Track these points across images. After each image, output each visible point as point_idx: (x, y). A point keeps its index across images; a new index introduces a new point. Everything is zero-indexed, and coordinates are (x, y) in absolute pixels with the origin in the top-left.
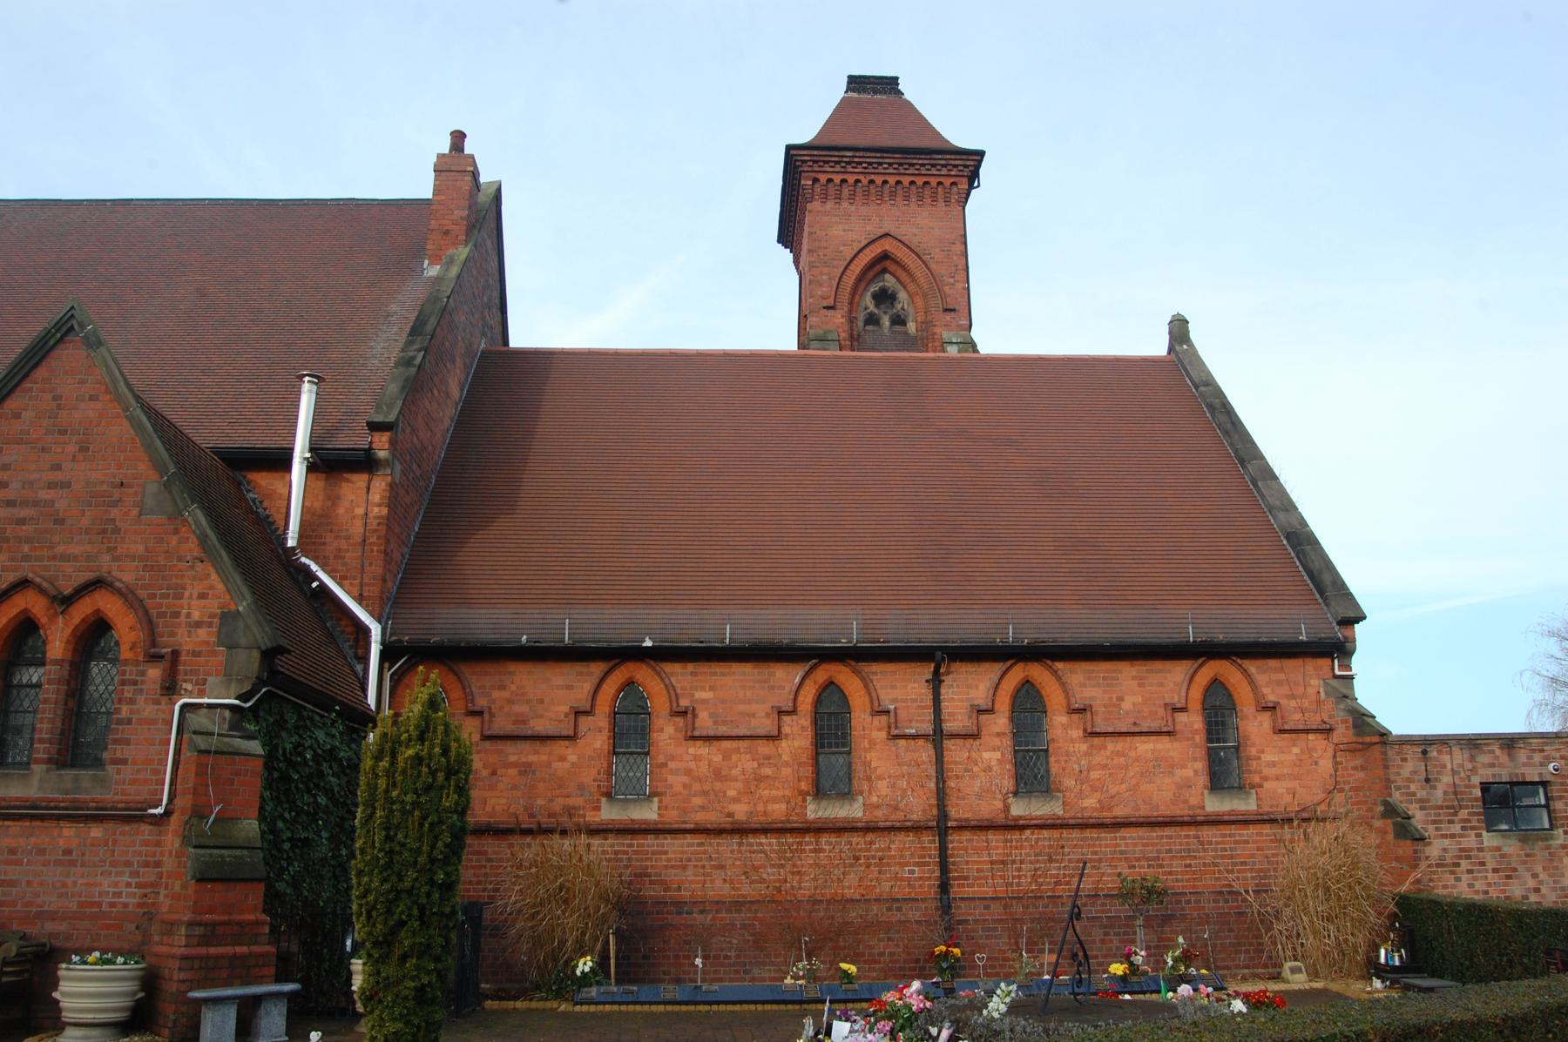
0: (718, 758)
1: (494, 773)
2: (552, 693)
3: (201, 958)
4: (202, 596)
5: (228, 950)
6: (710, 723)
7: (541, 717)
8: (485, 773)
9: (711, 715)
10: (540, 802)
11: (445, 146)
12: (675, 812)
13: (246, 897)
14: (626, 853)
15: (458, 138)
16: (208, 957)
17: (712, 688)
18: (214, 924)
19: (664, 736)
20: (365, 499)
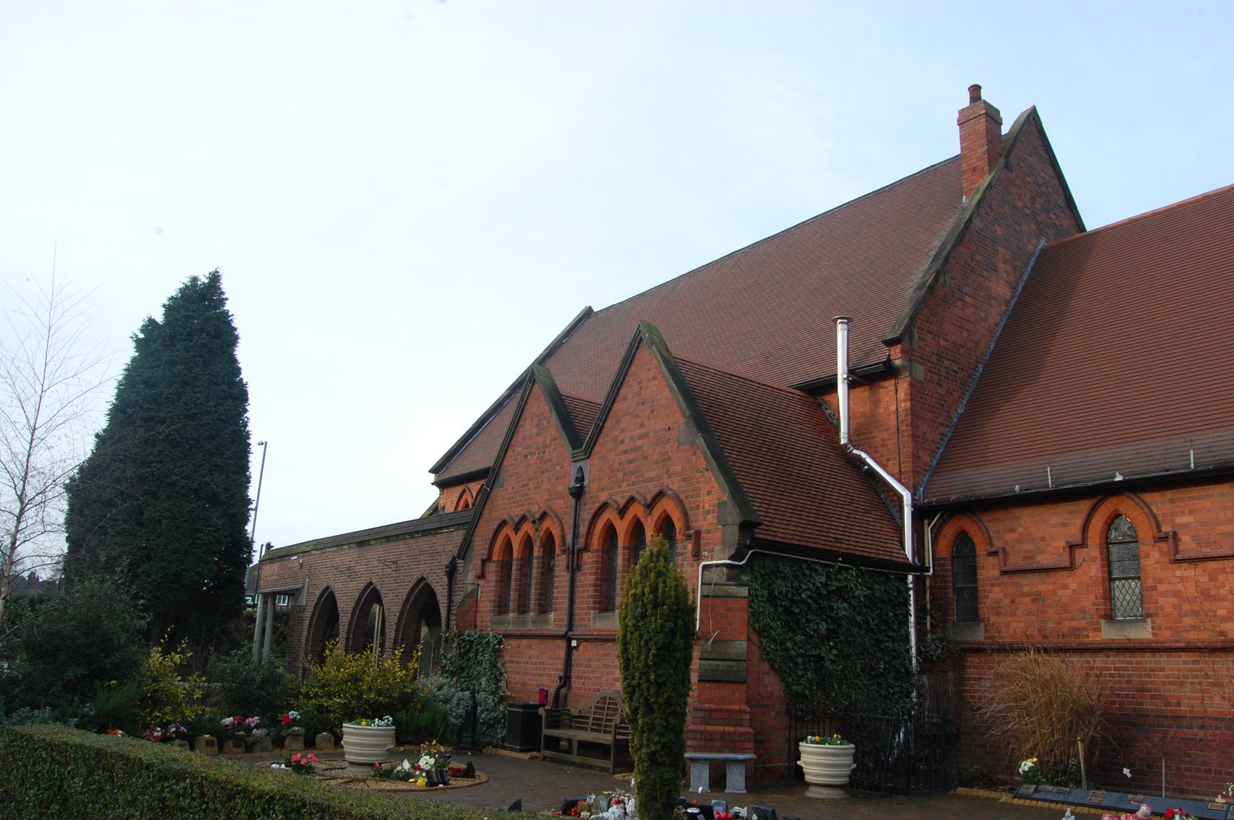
0: (1204, 579)
1: (1013, 602)
2: (1051, 530)
3: (701, 732)
4: (709, 493)
5: (720, 728)
6: (1193, 546)
7: (1044, 552)
8: (1006, 602)
9: (1193, 538)
10: (1051, 625)
11: (965, 102)
12: (1168, 632)
13: (734, 693)
14: (1126, 669)
15: (975, 91)
16: (706, 732)
17: (1191, 512)
18: (711, 710)
19: (1151, 561)
20: (894, 398)
